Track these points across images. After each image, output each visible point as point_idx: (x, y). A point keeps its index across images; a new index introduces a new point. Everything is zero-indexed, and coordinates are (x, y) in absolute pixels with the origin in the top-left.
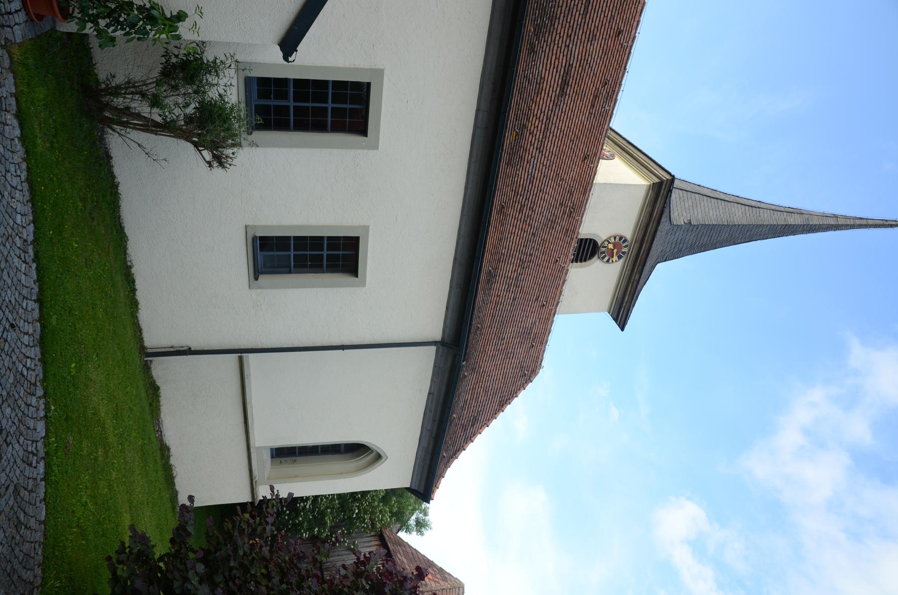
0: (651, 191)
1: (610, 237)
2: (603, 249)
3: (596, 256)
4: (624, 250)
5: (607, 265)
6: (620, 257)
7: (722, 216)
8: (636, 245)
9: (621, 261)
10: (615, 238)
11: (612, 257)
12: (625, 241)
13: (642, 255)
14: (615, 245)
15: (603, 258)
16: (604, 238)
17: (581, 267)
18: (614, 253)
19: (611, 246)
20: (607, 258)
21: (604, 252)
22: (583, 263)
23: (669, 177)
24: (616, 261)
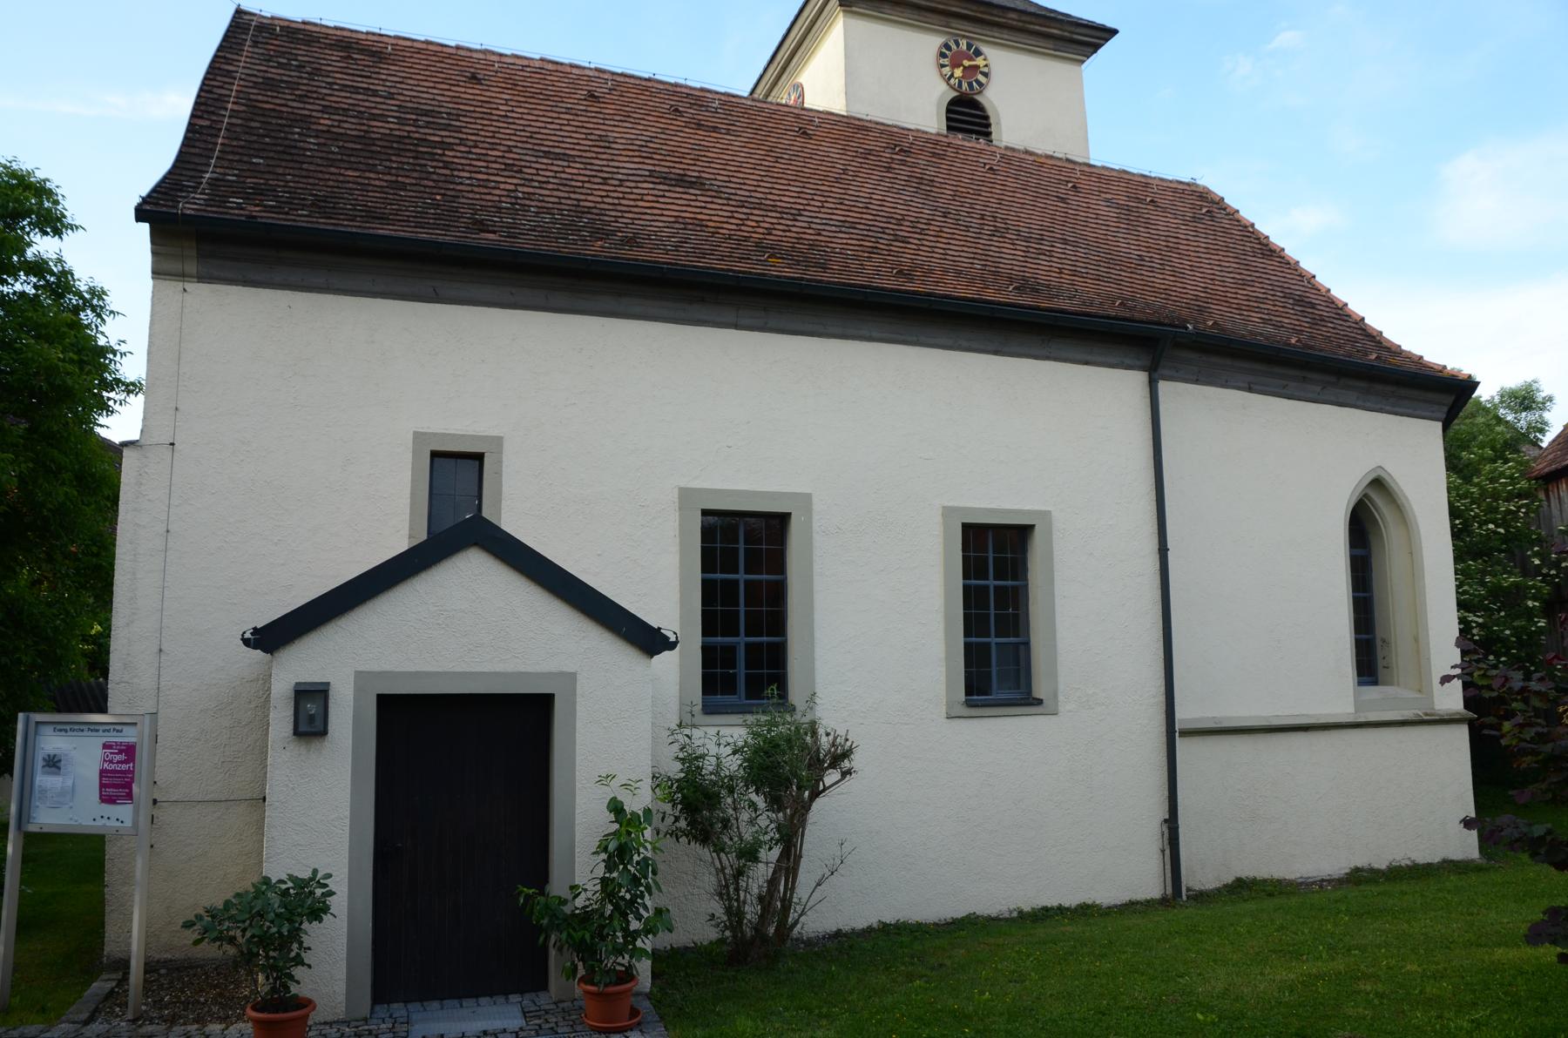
0: (854, 9)
3: (978, 98)
15: (980, 84)
16: (943, 86)
20: (981, 78)
21: (970, 84)
22: (992, 121)
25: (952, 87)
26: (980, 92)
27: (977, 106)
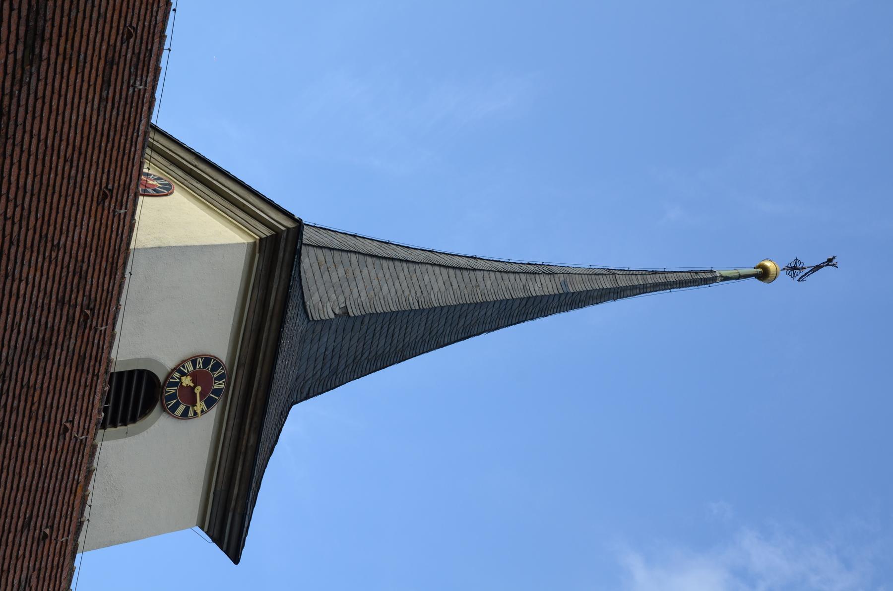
0: (257, 255)
1: (183, 363)
2: (172, 390)
3: (157, 408)
4: (219, 385)
5: (183, 423)
6: (210, 403)
7: (407, 293)
8: (241, 372)
9: (214, 412)
10: (194, 362)
11: (194, 403)
12: (218, 365)
13: (257, 391)
14: (195, 377)
17: (127, 434)
18: (196, 394)
19: (187, 381)
21: (173, 396)
22: (130, 426)
23: (290, 224)
24: (202, 411)
25: (169, 375)
26: (164, 409)
27: (147, 409)
